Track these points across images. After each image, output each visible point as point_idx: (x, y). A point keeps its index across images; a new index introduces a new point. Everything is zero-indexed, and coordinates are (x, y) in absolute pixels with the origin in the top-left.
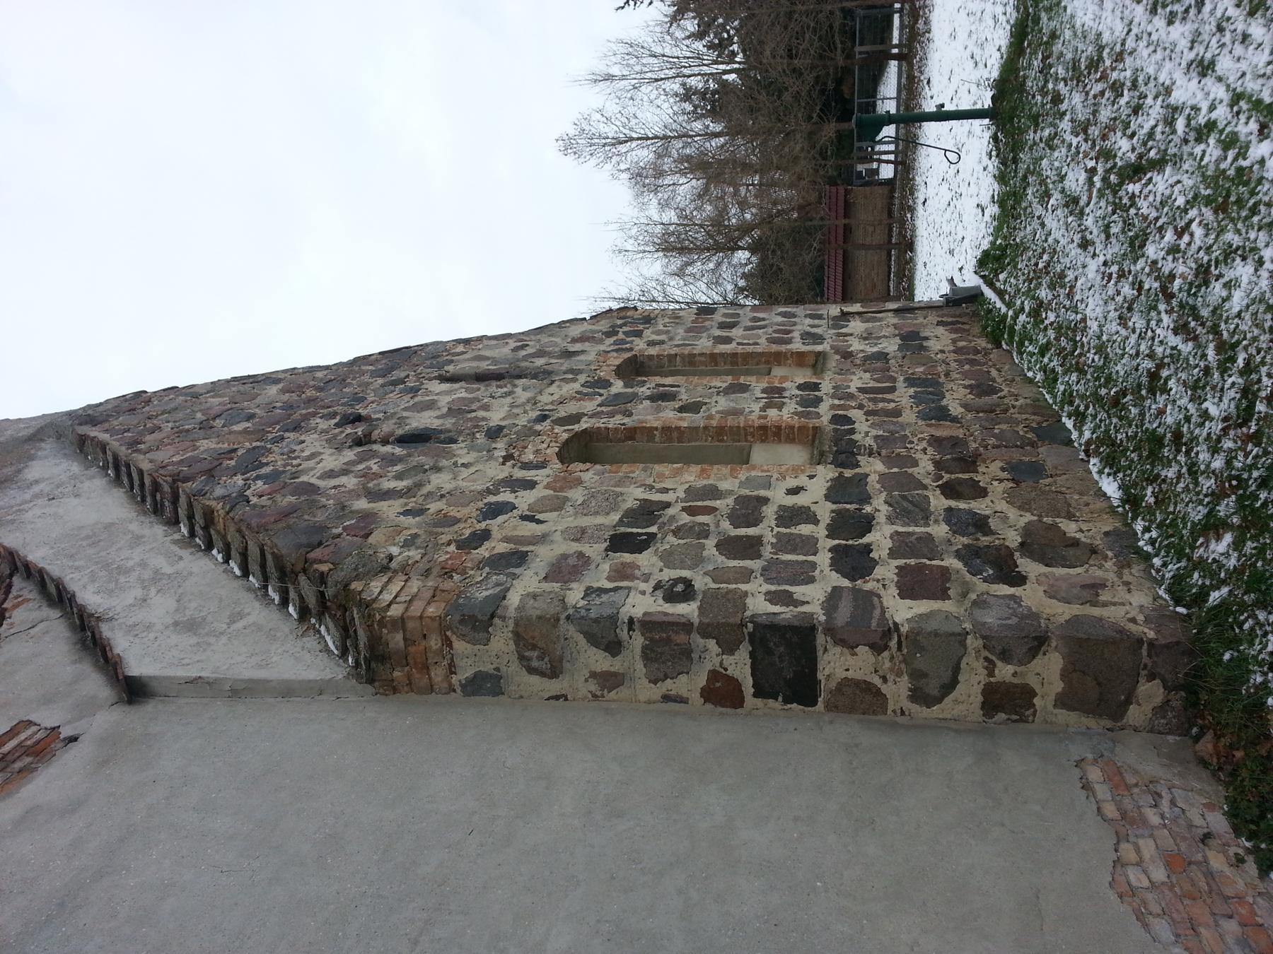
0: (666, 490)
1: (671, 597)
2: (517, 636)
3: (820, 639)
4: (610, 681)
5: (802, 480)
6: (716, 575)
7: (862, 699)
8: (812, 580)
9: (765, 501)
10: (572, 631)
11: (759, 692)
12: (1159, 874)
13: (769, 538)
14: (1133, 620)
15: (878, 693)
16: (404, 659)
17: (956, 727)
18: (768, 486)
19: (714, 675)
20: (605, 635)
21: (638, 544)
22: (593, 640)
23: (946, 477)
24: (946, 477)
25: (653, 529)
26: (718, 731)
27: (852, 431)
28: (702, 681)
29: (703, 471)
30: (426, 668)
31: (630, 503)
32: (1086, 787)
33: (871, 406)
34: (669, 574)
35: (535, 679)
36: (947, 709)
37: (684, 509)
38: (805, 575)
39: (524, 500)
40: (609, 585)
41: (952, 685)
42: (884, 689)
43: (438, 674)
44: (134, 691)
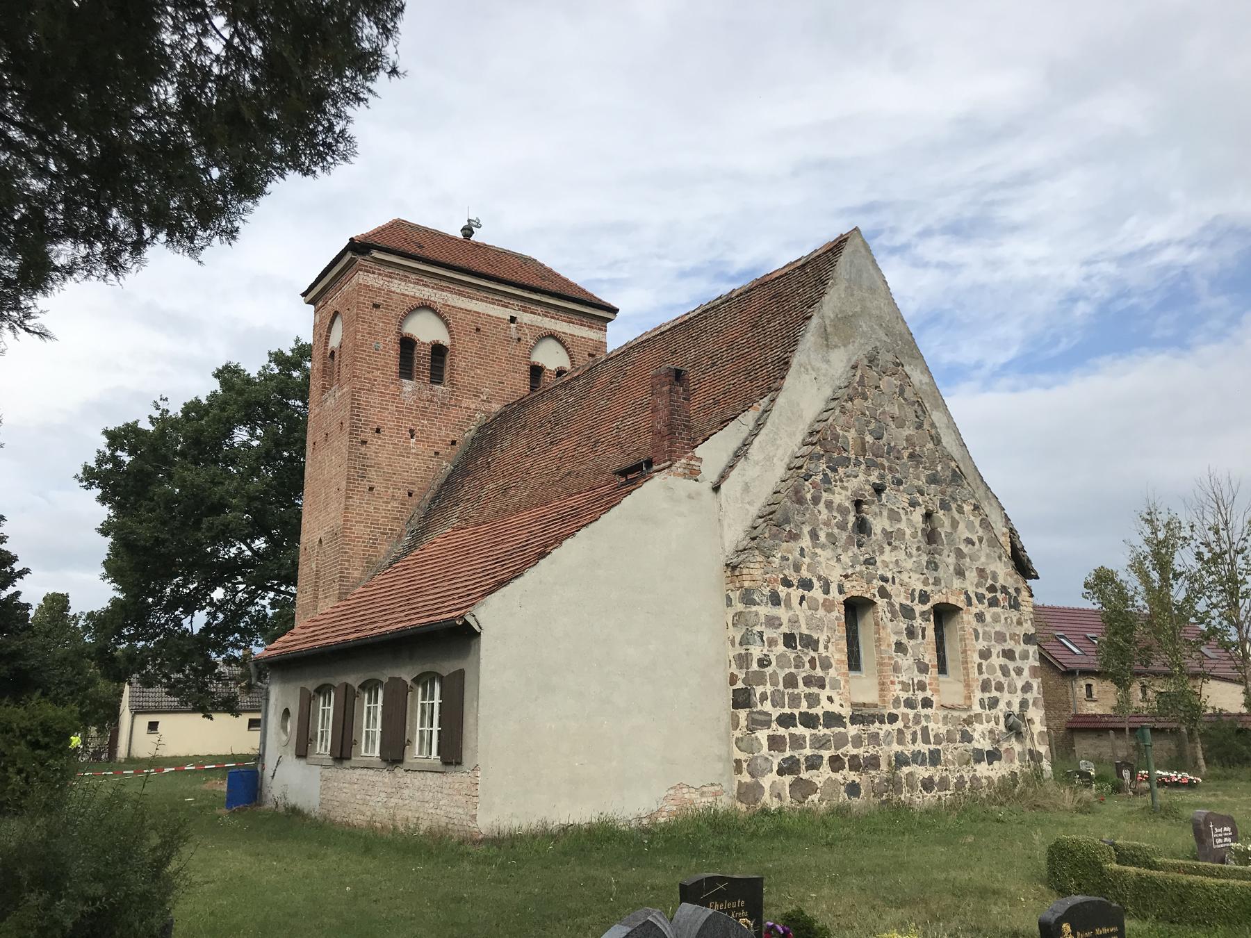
0: (826, 648)
8: (774, 706)
31: (815, 636)
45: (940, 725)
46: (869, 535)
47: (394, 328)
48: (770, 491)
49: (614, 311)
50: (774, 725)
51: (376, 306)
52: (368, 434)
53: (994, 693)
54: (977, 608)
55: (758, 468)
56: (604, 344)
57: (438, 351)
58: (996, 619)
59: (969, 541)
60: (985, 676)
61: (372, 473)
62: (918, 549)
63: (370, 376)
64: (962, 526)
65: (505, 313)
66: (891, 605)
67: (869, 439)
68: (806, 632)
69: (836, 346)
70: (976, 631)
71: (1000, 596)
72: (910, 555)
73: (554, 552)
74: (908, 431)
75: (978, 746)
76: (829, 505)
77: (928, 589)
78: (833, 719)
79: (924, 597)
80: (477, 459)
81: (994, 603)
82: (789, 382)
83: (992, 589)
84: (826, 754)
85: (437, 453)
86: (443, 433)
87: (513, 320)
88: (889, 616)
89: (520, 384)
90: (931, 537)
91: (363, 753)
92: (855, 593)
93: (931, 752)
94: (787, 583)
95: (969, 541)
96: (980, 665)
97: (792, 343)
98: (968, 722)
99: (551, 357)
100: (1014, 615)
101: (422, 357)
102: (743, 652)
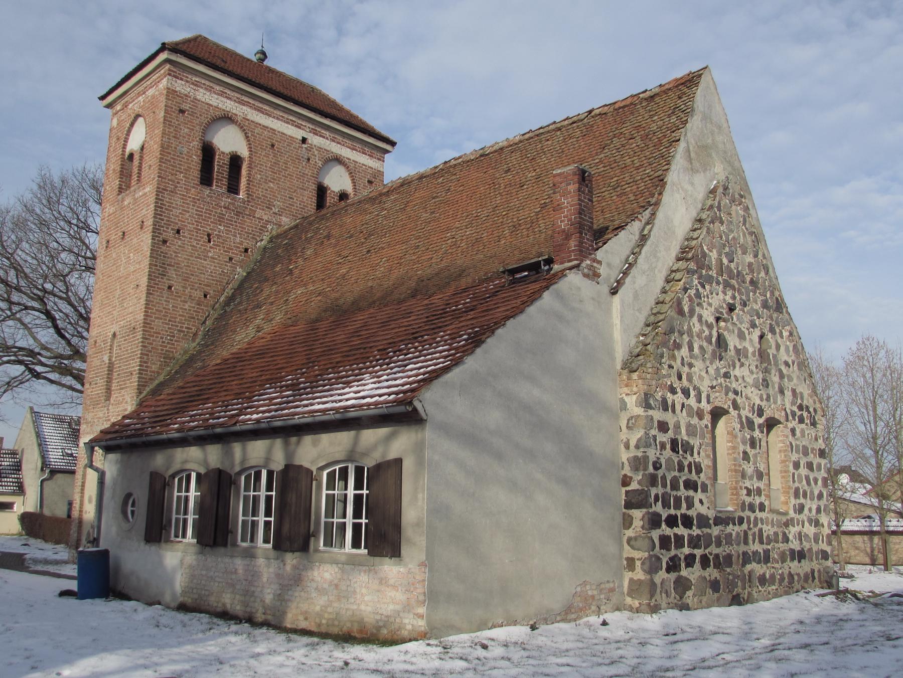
0: (699, 453)
1: (654, 464)
5: (706, 505)
6: (664, 478)
8: (664, 507)
9: (696, 491)
11: (627, 492)
13: (679, 494)
15: (629, 527)
16: (629, 379)
18: (703, 491)
19: (631, 478)
21: (674, 449)
23: (711, 558)
25: (681, 452)
27: (734, 524)
29: (709, 467)
30: (627, 386)
31: (692, 442)
32: (608, 582)
33: (750, 533)
34: (663, 461)
35: (626, 422)
36: (626, 547)
37: (690, 463)
38: (666, 505)
39: (692, 401)
42: (631, 529)
45: (769, 527)
46: (726, 351)
47: (198, 134)
48: (652, 302)
49: (393, 144)
50: (664, 526)
51: (182, 111)
52: (169, 234)
53: (802, 500)
54: (793, 424)
55: (644, 277)
56: (381, 174)
57: (235, 161)
59: (787, 364)
60: (797, 484)
61: (172, 273)
62: (757, 367)
63: (173, 177)
64: (782, 349)
65: (299, 134)
66: (740, 416)
67: (725, 261)
68: (685, 438)
69: (697, 171)
70: (791, 444)
71: (805, 414)
72: (752, 372)
73: (489, 340)
74: (749, 258)
75: (793, 547)
76: (700, 317)
77: (763, 404)
78: (703, 521)
79: (760, 413)
80: (274, 266)
81: (801, 420)
82: (666, 198)
83: (800, 408)
84: (698, 552)
85: (231, 259)
86: (238, 240)
87: (304, 140)
89: (309, 198)
90: (762, 355)
91: (173, 538)
92: (719, 404)
93: (764, 551)
94: (673, 391)
95: (787, 364)
96: (794, 474)
97: (667, 161)
98: (786, 524)
99: (337, 181)
100: (811, 432)
101: (220, 167)
102: (640, 454)
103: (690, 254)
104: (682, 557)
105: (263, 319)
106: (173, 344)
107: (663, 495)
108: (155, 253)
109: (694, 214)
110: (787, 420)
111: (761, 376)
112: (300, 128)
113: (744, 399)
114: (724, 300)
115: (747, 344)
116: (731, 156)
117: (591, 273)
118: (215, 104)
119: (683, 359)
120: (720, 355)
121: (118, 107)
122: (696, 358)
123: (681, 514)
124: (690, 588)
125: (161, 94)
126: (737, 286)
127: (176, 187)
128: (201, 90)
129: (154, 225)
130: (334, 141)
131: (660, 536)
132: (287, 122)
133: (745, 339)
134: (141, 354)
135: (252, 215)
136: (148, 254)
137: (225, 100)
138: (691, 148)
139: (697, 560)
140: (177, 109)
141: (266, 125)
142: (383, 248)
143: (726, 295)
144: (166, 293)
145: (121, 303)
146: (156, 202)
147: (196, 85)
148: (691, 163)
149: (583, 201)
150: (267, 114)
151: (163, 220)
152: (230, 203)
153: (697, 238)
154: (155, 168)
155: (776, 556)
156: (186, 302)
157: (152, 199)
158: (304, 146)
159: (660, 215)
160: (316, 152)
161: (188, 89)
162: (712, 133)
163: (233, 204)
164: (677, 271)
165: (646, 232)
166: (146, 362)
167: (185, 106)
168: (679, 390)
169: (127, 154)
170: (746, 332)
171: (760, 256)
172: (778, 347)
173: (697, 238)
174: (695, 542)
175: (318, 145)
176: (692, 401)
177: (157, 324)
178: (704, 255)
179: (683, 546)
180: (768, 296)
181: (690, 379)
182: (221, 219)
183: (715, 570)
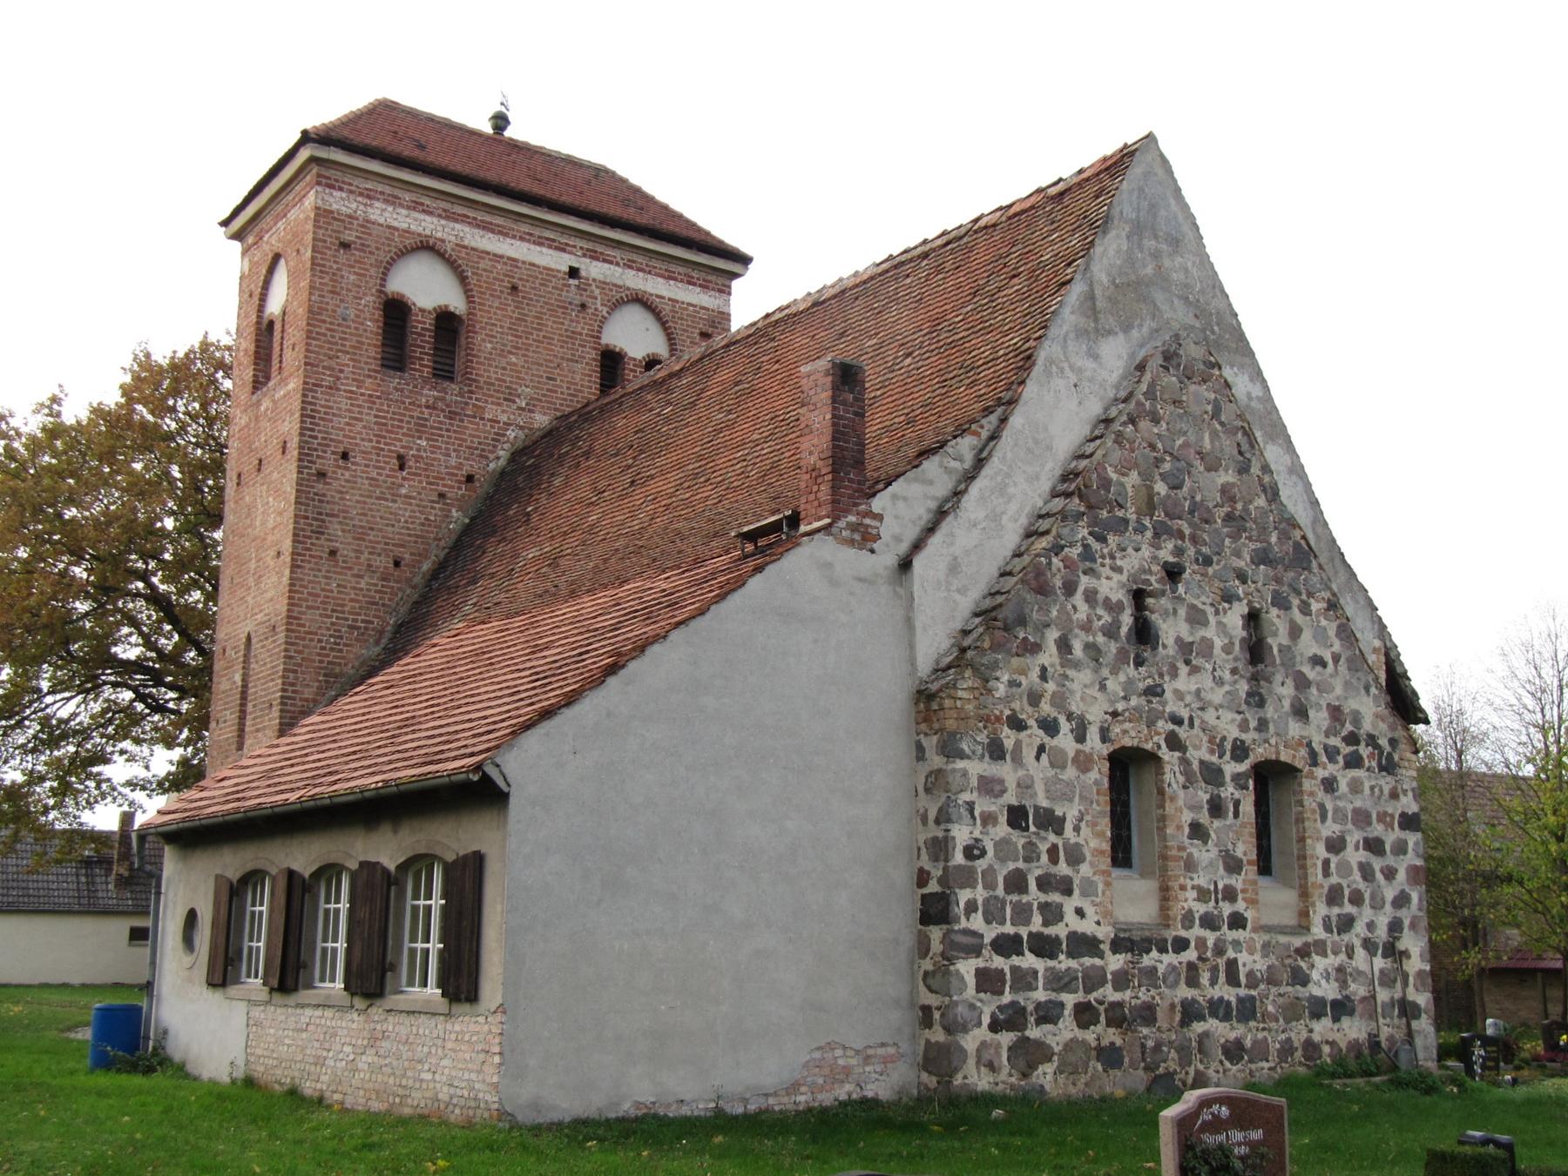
2: (940, 771)
3: (945, 927)
4: (924, 819)
6: (989, 873)
7: (923, 948)
8: (988, 922)
10: (943, 799)
11: (923, 896)
12: (841, 1062)
14: (965, 1077)
17: (913, 992)
20: (943, 818)
22: (940, 810)
23: (1102, 1008)
24: (1102, 1008)
25: (1032, 828)
26: (902, 877)
28: (927, 868)
29: (1102, 852)
32: (883, 1045)
36: (922, 988)
39: (1065, 740)
40: (977, 813)
41: (932, 991)
43: (923, 727)
44: (905, 565)
45: (1257, 957)
46: (1155, 648)
47: (374, 283)
51: (345, 246)
52: (328, 462)
53: (1349, 908)
57: (446, 322)
58: (1355, 787)
59: (1318, 661)
60: (1334, 879)
61: (335, 528)
62: (1234, 671)
65: (561, 262)
66: (1185, 761)
68: (1045, 803)
69: (1110, 332)
71: (1364, 751)
72: (1219, 682)
74: (1227, 477)
76: (1091, 597)
77: (1248, 737)
78: (1083, 944)
81: (1354, 762)
83: (1352, 739)
86: (453, 461)
87: (573, 272)
88: (1181, 779)
89: (583, 380)
90: (1256, 651)
92: (1127, 742)
94: (1017, 725)
95: (1318, 661)
99: (634, 336)
100: (1386, 783)
102: (940, 834)
103: (1079, 487)
104: (1030, 1008)
105: (475, 604)
106: (341, 651)
107: (987, 901)
108: (304, 495)
109: (1095, 408)
110: (1315, 763)
111: (1243, 687)
112: (564, 250)
113: (1197, 730)
114: (1155, 558)
115: (1210, 632)
116: (1202, 291)
117: (857, 537)
118: (405, 226)
119: (1044, 669)
120: (1137, 656)
121: (250, 240)
122: (1077, 665)
123: (1030, 934)
124: (1050, 1060)
125: (307, 218)
126: (1187, 532)
127: (338, 378)
128: (377, 204)
129: (301, 448)
130: (631, 267)
131: (977, 970)
132: (539, 242)
133: (1205, 623)
134: (285, 670)
135: (479, 414)
136: (293, 498)
137: (422, 216)
138: (1098, 292)
139: (1066, 1012)
140: (336, 243)
141: (500, 252)
142: (652, 477)
143: (1159, 548)
144: (325, 565)
145: (258, 583)
146: (303, 409)
147: (369, 197)
148: (1096, 320)
149: (841, 418)
150: (500, 233)
151: (316, 438)
152: (436, 398)
153: (1091, 455)
154: (301, 347)
155: (1270, 1008)
156: (361, 577)
157: (296, 404)
158: (571, 281)
159: (1016, 420)
160: (597, 292)
161: (354, 206)
162: (1156, 255)
163: (443, 399)
164: (1048, 515)
165: (985, 454)
166: (292, 684)
167: (349, 236)
168: (1032, 722)
169: (265, 322)
170: (1210, 610)
171: (1255, 470)
172: (1295, 632)
173: (1091, 455)
174: (1060, 982)
175: (600, 277)
176: (1065, 740)
177: (311, 618)
178: (1106, 484)
179: (1031, 987)
180: (1274, 539)
181: (1059, 700)
182: (421, 427)
183: (1111, 1030)
